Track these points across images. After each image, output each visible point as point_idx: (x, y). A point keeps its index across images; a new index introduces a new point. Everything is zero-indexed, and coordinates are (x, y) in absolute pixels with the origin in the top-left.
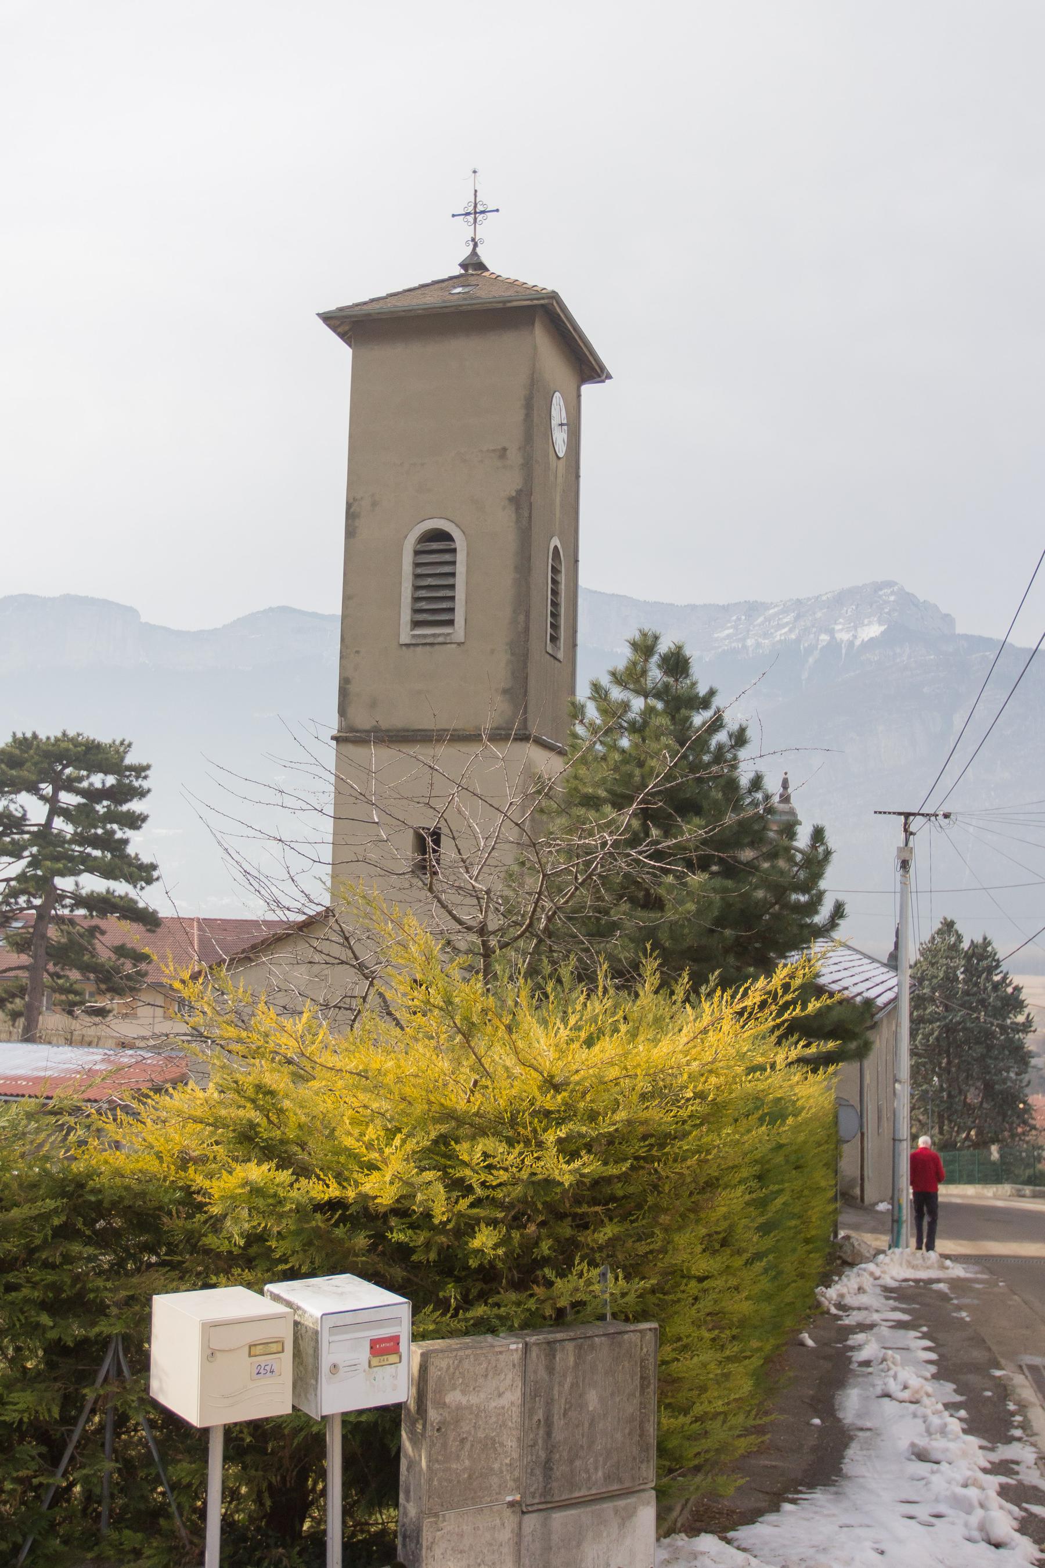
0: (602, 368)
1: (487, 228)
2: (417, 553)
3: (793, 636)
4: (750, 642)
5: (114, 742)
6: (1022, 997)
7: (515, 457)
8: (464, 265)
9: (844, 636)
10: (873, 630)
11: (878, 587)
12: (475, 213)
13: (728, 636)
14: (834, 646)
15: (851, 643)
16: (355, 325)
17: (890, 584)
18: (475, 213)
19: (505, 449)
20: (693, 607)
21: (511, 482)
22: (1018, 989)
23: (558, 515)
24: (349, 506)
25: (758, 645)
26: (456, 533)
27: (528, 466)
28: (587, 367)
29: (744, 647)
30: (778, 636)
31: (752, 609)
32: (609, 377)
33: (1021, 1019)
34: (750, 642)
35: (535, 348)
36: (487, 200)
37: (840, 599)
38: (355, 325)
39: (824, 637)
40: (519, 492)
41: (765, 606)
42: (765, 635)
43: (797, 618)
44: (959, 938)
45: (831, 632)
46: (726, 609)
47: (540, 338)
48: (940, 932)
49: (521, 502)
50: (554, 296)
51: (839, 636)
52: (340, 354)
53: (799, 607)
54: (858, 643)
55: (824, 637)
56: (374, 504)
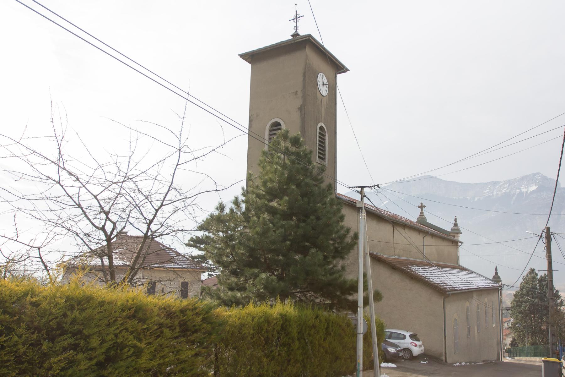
0: (344, 67)
1: (300, 23)
2: (270, 131)
3: (508, 191)
4: (495, 193)
5: (221, 207)
6: (559, 294)
7: (300, 94)
8: (292, 36)
9: (524, 190)
10: (533, 188)
11: (535, 174)
12: (297, 18)
13: (488, 192)
14: (521, 193)
15: (527, 192)
16: (252, 57)
17: (538, 173)
18: (297, 18)
19: (297, 92)
20: (476, 184)
21: (299, 102)
22: (557, 291)
23: (323, 115)
24: (250, 117)
25: (497, 194)
26: (282, 123)
27: (304, 97)
28: (339, 68)
29: (493, 195)
30: (503, 191)
31: (495, 183)
32: (347, 70)
33: (559, 301)
34: (495, 193)
35: (307, 56)
36: (300, 13)
37: (523, 179)
38: (252, 57)
39: (518, 191)
40: (301, 105)
41: (499, 182)
42: (499, 191)
43: (509, 185)
44: (536, 274)
45: (520, 189)
46: (486, 184)
47: (309, 51)
48: (529, 273)
49: (302, 109)
50: (310, 36)
51: (522, 190)
52: (247, 67)
53: (509, 182)
54: (529, 192)
55: (518, 191)
56: (257, 116)
